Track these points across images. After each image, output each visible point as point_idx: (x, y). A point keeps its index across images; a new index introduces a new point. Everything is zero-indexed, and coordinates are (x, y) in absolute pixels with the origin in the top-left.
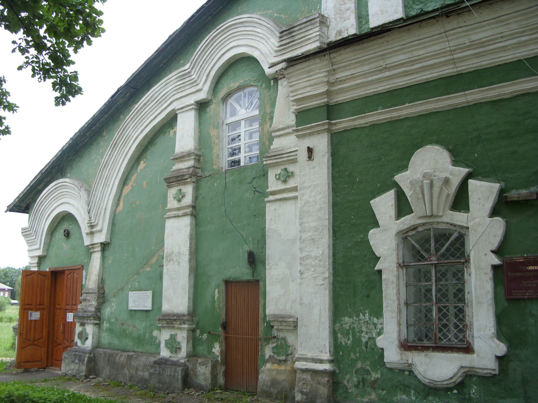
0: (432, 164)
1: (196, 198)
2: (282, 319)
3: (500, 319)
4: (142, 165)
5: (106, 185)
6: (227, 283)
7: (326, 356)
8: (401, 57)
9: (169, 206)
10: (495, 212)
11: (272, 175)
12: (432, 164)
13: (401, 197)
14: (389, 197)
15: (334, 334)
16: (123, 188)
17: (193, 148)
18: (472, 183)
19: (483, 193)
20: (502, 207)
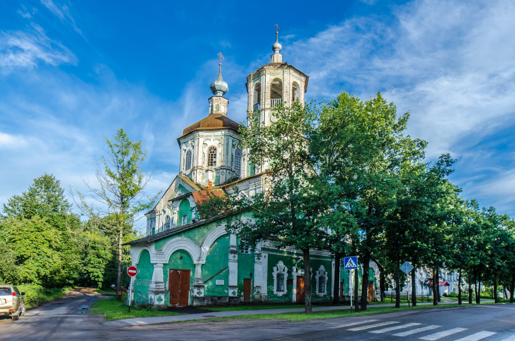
4: (216, 243)
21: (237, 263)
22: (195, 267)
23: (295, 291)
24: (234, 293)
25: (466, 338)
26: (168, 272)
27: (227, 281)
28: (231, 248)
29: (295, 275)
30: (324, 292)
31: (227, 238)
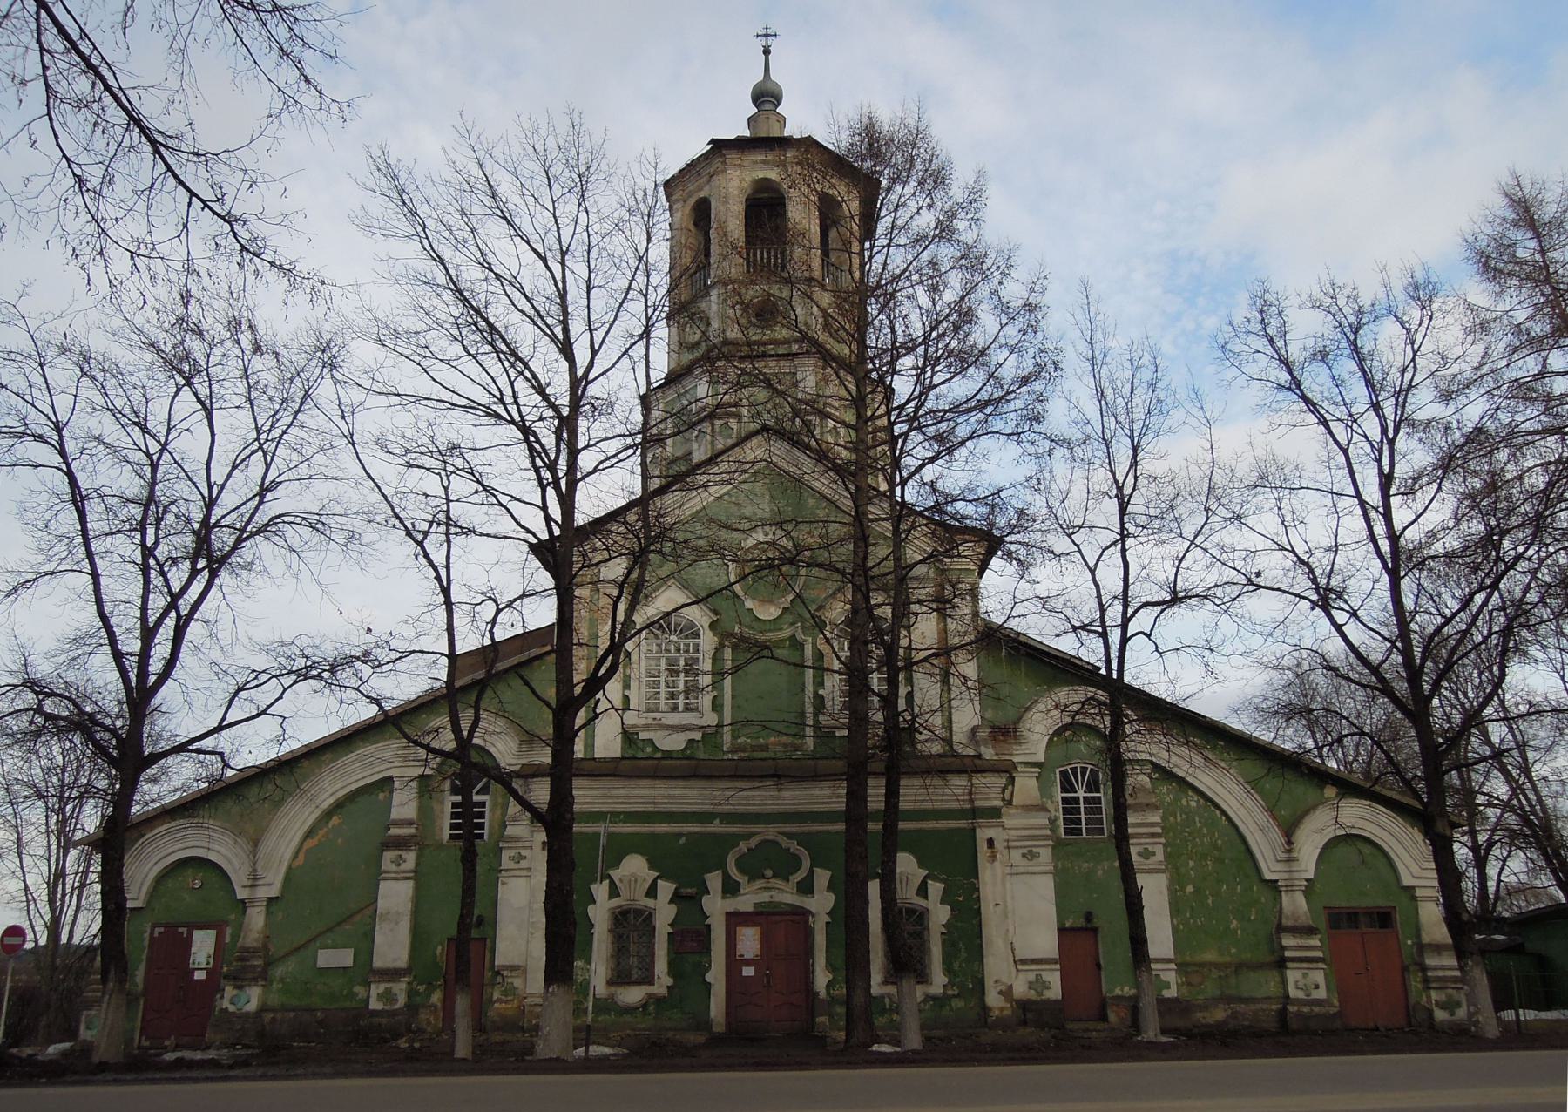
0: (635, 867)
1: (417, 864)
2: (513, 968)
3: (670, 964)
4: (335, 820)
9: (394, 815)
10: (671, 901)
11: (505, 855)
12: (635, 867)
13: (612, 883)
16: (464, 922)
17: (845, 144)
19: (666, 888)
20: (676, 898)
21: (411, 883)
22: (245, 909)
24: (387, 996)
26: (147, 935)
28: (394, 831)
29: (716, 906)
30: (648, 979)
31: (381, 796)
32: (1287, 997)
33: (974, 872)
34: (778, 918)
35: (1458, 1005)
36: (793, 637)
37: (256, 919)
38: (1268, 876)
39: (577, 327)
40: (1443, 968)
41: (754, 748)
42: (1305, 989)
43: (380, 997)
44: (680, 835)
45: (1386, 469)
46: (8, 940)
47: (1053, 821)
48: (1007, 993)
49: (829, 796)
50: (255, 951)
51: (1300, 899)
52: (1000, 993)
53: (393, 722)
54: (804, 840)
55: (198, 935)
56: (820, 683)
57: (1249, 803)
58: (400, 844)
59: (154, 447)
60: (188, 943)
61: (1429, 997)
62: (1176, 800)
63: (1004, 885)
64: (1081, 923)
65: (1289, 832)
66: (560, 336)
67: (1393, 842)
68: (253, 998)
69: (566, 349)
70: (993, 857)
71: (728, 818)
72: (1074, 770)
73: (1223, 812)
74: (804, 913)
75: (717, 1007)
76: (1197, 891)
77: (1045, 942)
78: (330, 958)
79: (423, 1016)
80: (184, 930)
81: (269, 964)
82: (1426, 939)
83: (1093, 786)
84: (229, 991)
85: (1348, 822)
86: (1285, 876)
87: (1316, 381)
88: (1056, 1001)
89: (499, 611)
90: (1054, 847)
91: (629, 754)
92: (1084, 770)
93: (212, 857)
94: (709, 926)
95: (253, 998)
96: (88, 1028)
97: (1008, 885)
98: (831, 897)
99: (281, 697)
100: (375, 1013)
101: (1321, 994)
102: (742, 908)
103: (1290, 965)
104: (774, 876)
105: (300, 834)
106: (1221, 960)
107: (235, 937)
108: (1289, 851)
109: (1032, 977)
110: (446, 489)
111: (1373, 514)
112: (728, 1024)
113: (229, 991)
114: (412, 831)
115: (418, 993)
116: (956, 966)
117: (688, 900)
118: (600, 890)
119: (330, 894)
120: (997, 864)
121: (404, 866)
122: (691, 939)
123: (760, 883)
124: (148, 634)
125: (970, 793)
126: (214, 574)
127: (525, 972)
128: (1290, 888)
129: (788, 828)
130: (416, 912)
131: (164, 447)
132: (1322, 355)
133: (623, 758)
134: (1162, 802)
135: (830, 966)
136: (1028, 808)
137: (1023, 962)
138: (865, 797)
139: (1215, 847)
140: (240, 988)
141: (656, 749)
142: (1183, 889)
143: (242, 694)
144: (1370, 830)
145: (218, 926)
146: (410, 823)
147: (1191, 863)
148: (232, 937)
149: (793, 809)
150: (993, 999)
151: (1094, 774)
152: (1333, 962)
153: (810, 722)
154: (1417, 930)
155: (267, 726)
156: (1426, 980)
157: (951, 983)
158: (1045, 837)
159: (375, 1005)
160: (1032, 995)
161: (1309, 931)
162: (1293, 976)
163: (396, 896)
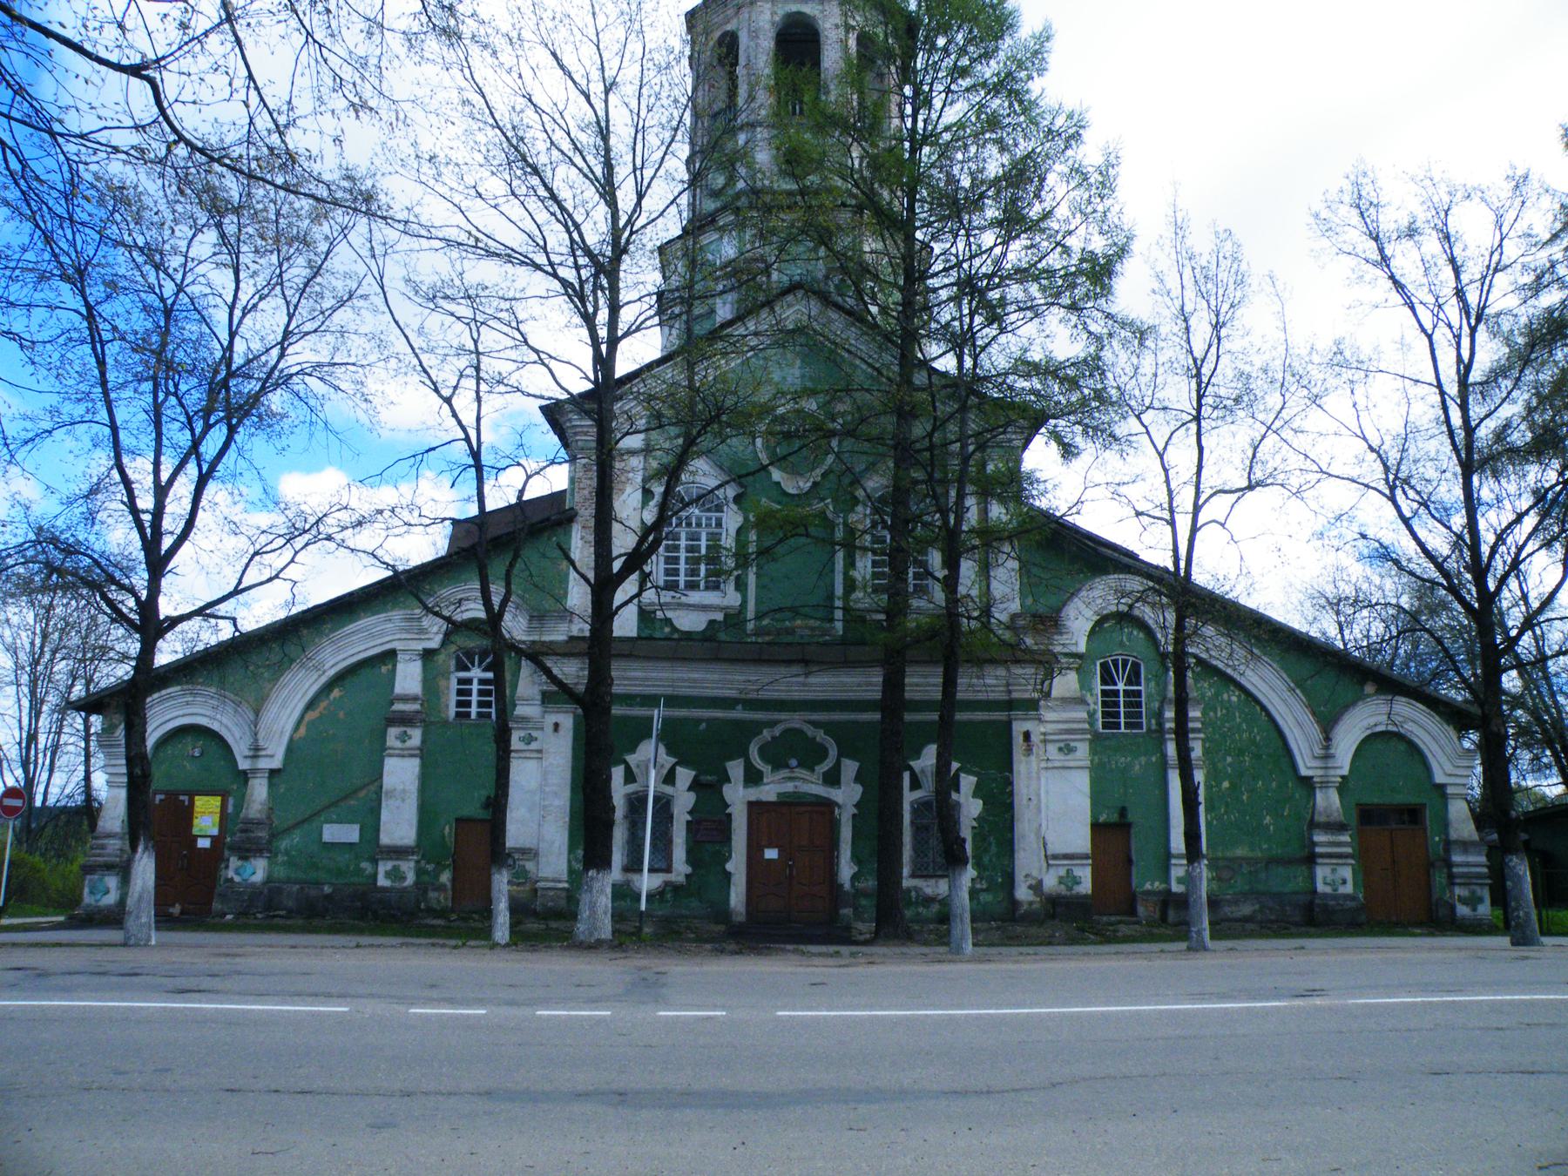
1: (423, 742)
2: (524, 851)
3: (689, 852)
4: (336, 693)
5: (283, 706)
6: (458, 820)
7: (565, 877)
8: (639, 674)
10: (690, 789)
14: (906, 776)
15: (569, 861)
18: (679, 769)
19: (685, 776)
20: (695, 786)
21: (416, 762)
22: (246, 781)
23: (737, 865)
24: (395, 874)
25: (1119, 542)
27: (371, 820)
28: (398, 707)
29: (737, 795)
31: (384, 669)
32: (1315, 891)
33: (1008, 765)
34: (803, 809)
35: (1481, 900)
36: (822, 514)
37: (259, 791)
38: (1304, 772)
39: (622, 172)
40: (1468, 865)
41: (779, 632)
42: (1332, 884)
43: (388, 875)
44: (699, 721)
45: (1466, 355)
46: (8, 802)
47: (1091, 715)
48: (1037, 887)
49: (866, 683)
50: (259, 823)
51: (1334, 797)
52: (1030, 887)
53: (402, 587)
54: (829, 728)
55: (201, 802)
56: (850, 563)
57: (1292, 700)
58: (405, 720)
59: (169, 289)
60: (187, 814)
61: (1452, 892)
62: (1217, 695)
63: (1039, 779)
64: (1115, 818)
65: (1327, 725)
66: (598, 171)
67: (1427, 738)
68: (257, 871)
69: (608, 191)
70: (1029, 751)
71: (751, 704)
72: (1115, 663)
73: (1264, 708)
74: (828, 805)
75: (737, 897)
76: (1233, 786)
77: (1080, 839)
78: (333, 832)
79: (432, 895)
80: (185, 798)
81: (274, 836)
82: (1453, 835)
83: (1134, 678)
84: (234, 862)
85: (1397, 719)
86: (1320, 772)
87: (1406, 260)
88: (1086, 896)
89: (529, 477)
90: (1091, 742)
91: (646, 633)
92: (1125, 663)
93: (215, 726)
94: (730, 815)
95: (257, 871)
96: (91, 892)
97: (1043, 780)
98: (859, 789)
99: (292, 561)
100: (384, 889)
101: (1348, 889)
102: (765, 798)
103: (1320, 861)
104: (800, 765)
105: (301, 706)
106: (1250, 855)
107: (239, 806)
108: (1327, 748)
109: (1062, 872)
110: (476, 342)
111: (1449, 402)
112: (748, 912)
113: (234, 862)
114: (416, 707)
115: (426, 872)
116: (986, 860)
117: (708, 789)
118: (618, 773)
119: (333, 766)
120: (1033, 758)
121: (409, 743)
122: (710, 829)
123: (784, 773)
124: (161, 491)
125: (1008, 685)
126: (232, 430)
127: (536, 854)
128: (1325, 785)
129: (815, 717)
130: (423, 789)
131: (180, 289)
132: (1411, 232)
133: (639, 638)
134: (1203, 695)
135: (856, 858)
136: (1066, 701)
137: (1055, 857)
138: (903, 684)
139: (1253, 742)
140: (244, 858)
141: (675, 629)
142: (1219, 784)
143: (257, 558)
144: (1411, 729)
145: (225, 795)
146: (415, 699)
147: (1229, 759)
148: (235, 806)
149: (821, 696)
150: (1023, 893)
151: (1136, 667)
152: (1364, 859)
153: (838, 603)
154: (1445, 824)
155: (280, 589)
156: (1451, 876)
157: (980, 877)
158: (1083, 731)
159: (382, 881)
160: (1062, 890)
161: (1340, 827)
162: (1322, 872)
163: (401, 774)
